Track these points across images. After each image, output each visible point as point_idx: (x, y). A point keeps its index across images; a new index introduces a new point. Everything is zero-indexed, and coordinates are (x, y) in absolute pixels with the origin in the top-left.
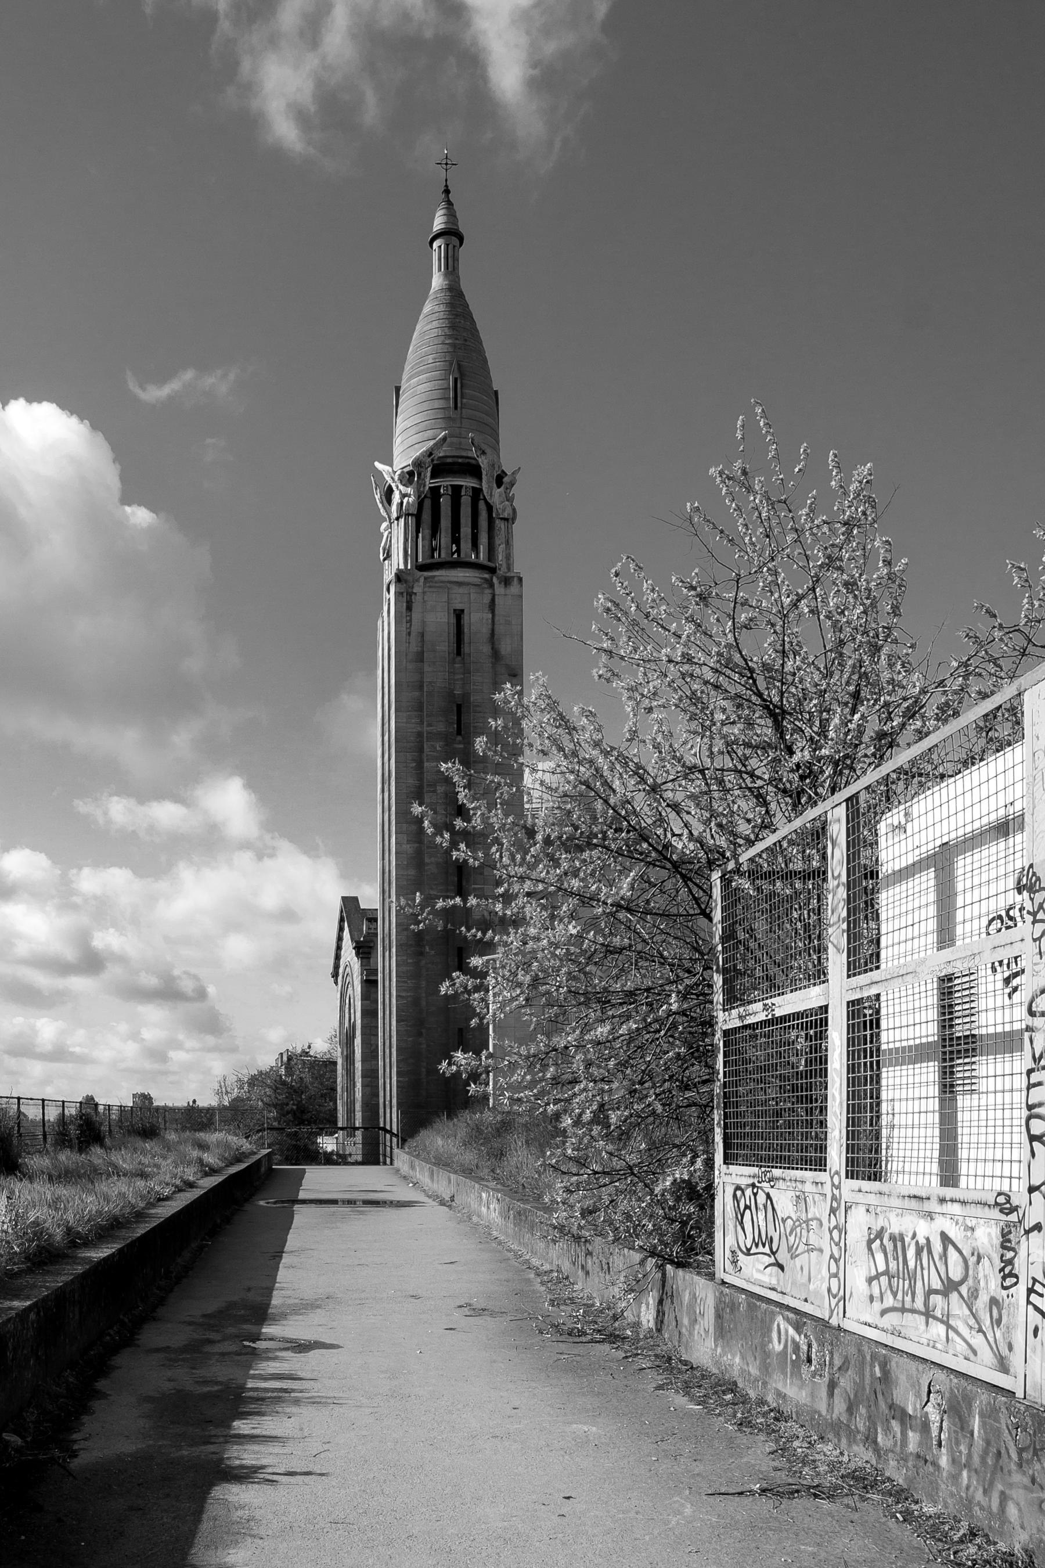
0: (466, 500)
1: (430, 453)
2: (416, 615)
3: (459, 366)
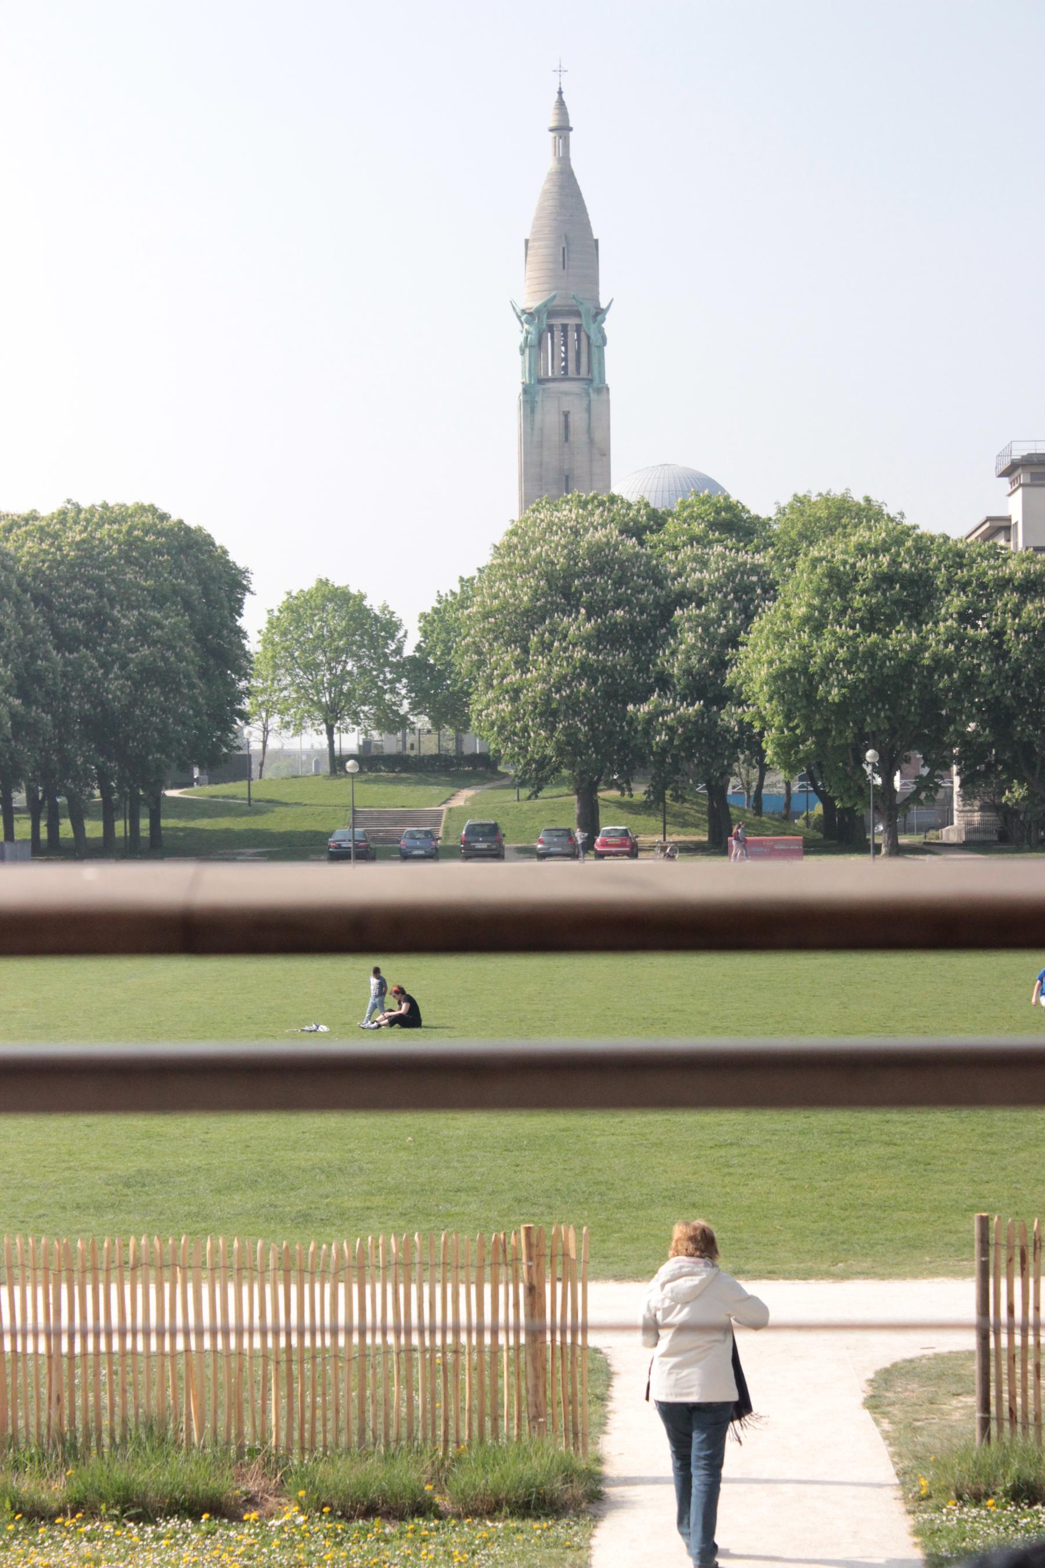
1: (545, 305)
2: (538, 417)
3: (566, 237)
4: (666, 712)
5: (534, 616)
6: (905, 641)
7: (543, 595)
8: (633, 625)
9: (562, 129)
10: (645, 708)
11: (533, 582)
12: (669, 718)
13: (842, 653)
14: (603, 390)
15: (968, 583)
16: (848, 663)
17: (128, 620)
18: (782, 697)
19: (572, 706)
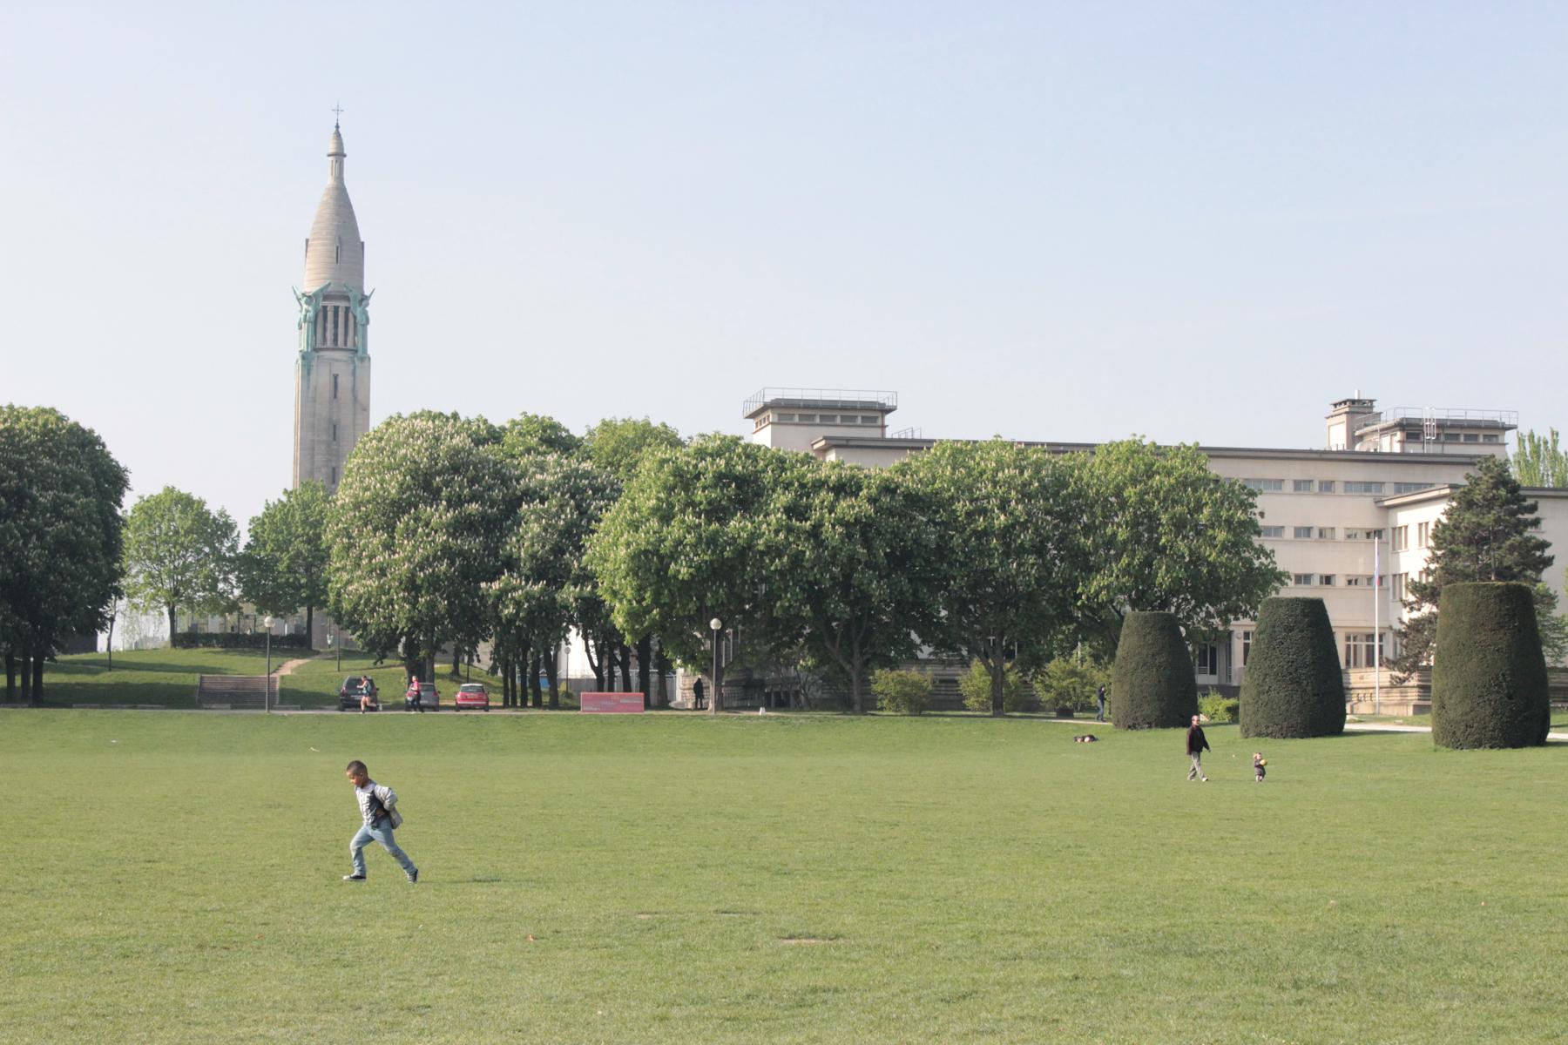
0: (330, 315)
4: (514, 589)
5: (400, 507)
6: (742, 529)
7: (409, 488)
8: (484, 516)
9: (339, 155)
10: (496, 585)
11: (400, 478)
12: (518, 594)
13: (690, 538)
14: (365, 359)
15: (790, 484)
16: (694, 546)
17: (46, 498)
18: (636, 574)
19: (434, 583)
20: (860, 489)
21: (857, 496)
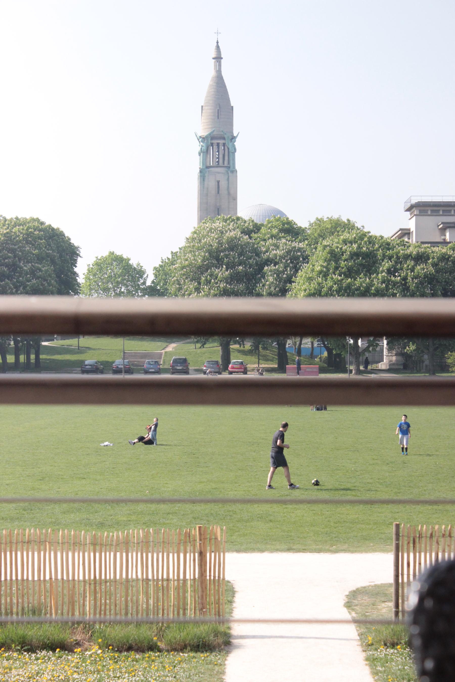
5: (202, 269)
9: (218, 58)
11: (203, 254)
13: (335, 287)
14: (234, 171)
20: (429, 259)
21: (426, 263)
